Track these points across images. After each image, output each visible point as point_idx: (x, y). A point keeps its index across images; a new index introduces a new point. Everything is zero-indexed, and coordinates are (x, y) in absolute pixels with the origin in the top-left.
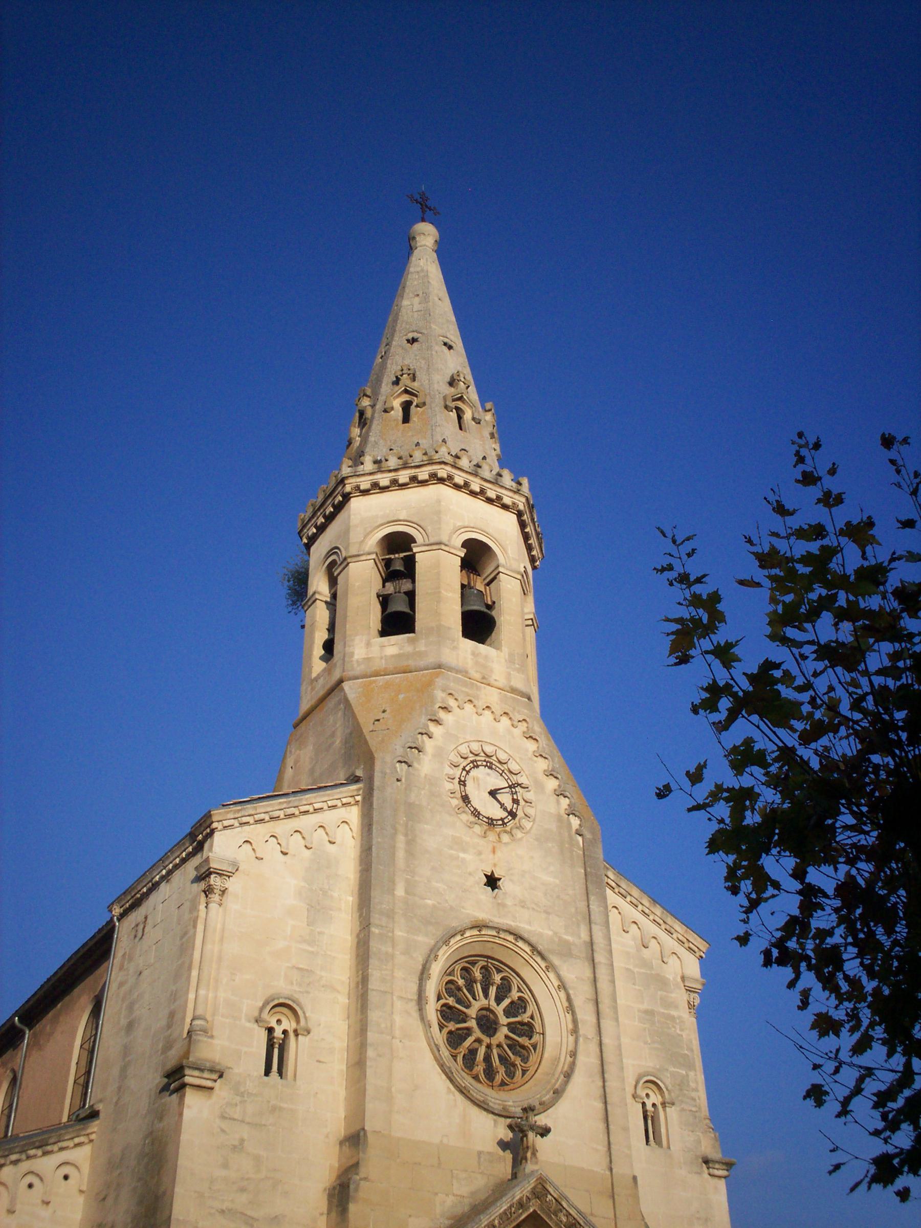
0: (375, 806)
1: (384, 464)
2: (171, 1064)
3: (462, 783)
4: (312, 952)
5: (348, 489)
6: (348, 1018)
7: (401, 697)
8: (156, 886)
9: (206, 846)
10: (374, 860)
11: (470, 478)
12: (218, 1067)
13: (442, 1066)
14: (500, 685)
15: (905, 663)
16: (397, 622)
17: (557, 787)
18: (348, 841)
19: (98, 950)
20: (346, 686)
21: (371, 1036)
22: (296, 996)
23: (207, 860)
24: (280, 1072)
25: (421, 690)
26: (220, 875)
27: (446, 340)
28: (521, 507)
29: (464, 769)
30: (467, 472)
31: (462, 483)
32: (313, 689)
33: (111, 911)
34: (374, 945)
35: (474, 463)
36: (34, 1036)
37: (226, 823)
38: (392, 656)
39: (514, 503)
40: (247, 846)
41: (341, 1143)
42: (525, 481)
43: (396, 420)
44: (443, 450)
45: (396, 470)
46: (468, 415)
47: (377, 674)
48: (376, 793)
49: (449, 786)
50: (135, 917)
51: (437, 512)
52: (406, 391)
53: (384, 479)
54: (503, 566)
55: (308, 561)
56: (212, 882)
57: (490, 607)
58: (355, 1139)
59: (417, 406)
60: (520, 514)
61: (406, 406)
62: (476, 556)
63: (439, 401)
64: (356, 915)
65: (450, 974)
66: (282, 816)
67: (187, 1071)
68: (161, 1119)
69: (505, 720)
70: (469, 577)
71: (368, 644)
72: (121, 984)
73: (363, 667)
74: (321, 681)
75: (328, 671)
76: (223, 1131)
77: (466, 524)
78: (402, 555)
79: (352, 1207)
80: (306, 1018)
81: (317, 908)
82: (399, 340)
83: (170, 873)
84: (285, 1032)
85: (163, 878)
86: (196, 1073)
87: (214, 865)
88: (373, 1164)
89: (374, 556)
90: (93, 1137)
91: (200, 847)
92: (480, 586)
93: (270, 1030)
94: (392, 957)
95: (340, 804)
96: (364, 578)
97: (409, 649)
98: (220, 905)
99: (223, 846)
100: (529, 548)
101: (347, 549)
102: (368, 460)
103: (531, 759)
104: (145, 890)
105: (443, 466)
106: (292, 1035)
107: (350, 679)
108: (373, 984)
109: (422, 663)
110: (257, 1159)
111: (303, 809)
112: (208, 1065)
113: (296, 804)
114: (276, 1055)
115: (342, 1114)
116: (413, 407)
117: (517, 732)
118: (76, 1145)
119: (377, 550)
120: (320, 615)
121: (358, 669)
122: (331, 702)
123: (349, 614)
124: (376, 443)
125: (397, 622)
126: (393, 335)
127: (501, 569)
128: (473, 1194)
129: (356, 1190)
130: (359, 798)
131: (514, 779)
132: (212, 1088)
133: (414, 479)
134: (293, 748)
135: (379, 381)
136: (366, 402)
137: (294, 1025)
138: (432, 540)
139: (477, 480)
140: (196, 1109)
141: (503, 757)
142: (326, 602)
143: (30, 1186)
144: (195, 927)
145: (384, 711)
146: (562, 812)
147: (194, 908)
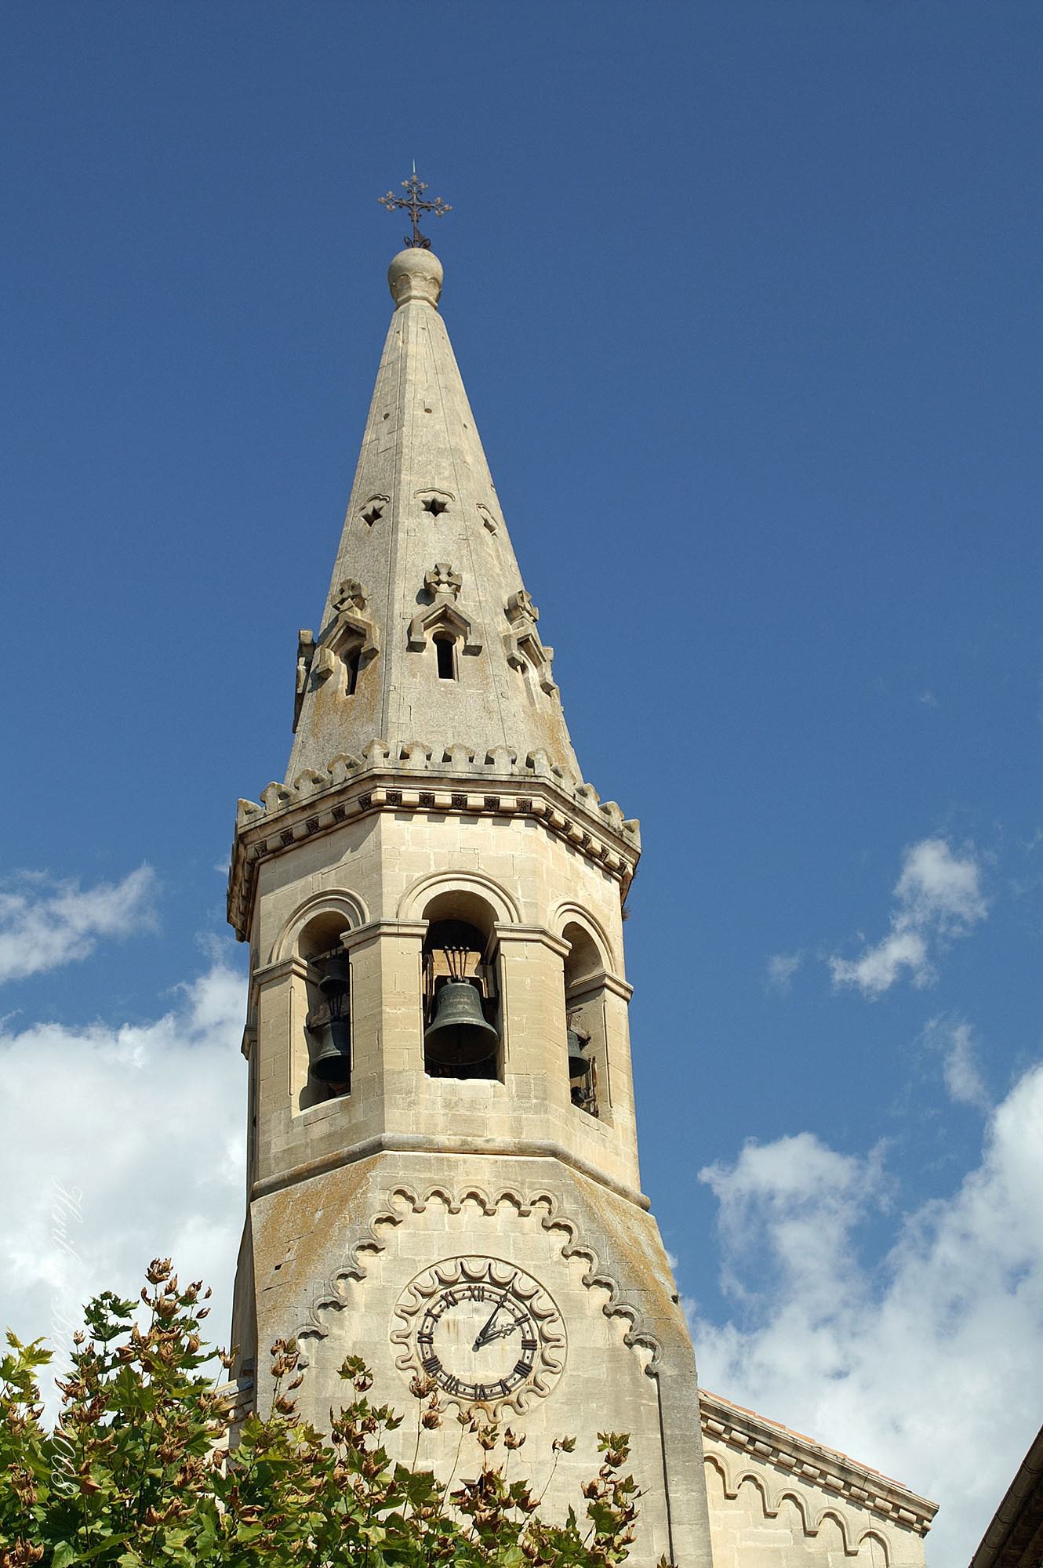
3: (425, 1338)
15: (801, 1208)
77: (433, 870)
82: (355, 520)
97: (342, 1121)
103: (558, 1263)
117: (532, 1222)
146: (620, 1343)
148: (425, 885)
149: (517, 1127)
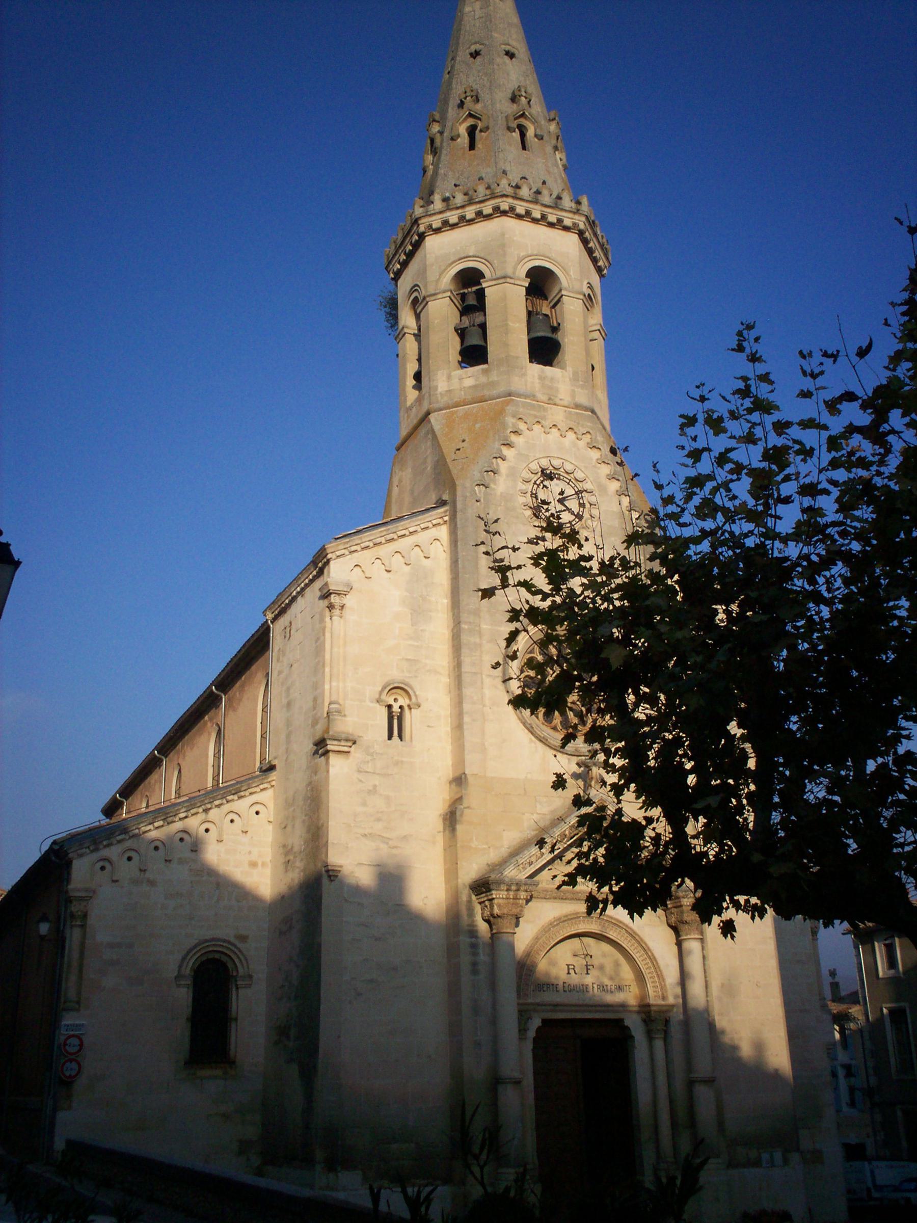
0: (459, 526)
1: (452, 201)
2: (318, 736)
4: (417, 646)
5: (422, 229)
6: (450, 692)
7: (478, 426)
8: (294, 599)
9: (326, 571)
10: (460, 570)
11: (531, 206)
12: (351, 738)
13: (524, 724)
14: (566, 403)
16: (474, 354)
17: (618, 488)
18: (440, 554)
19: (257, 647)
20: (432, 417)
21: (466, 707)
22: (407, 680)
23: (326, 584)
24: (400, 737)
25: (494, 418)
26: (339, 594)
27: (508, 48)
28: (582, 226)
29: (535, 483)
30: (527, 201)
31: (523, 213)
32: (408, 417)
33: (265, 615)
34: (465, 638)
35: (534, 189)
36: (229, 700)
37: (338, 553)
38: (470, 387)
39: (574, 224)
40: (357, 569)
41: (450, 783)
42: (585, 200)
43: (463, 148)
44: (504, 182)
45: (463, 207)
46: (530, 133)
47: (457, 405)
48: (459, 515)
49: (522, 500)
50: (283, 621)
51: (502, 244)
52: (470, 115)
53: (453, 217)
54: (566, 289)
55: (396, 294)
56: (332, 601)
57: (555, 329)
58: (459, 780)
59: (481, 131)
60: (581, 233)
61: (472, 131)
62: (540, 283)
63: (501, 122)
64: (451, 614)
65: (531, 652)
66: (384, 542)
67: (328, 742)
68: (316, 773)
69: (571, 436)
70: (532, 303)
71: (449, 377)
72: (280, 673)
73: (445, 399)
74: (414, 410)
75: (419, 400)
76: (361, 781)
77: (530, 252)
78: (474, 289)
79: (459, 827)
80: (416, 696)
81: (418, 611)
82: (463, 55)
83: (303, 589)
84: (401, 707)
85: (298, 593)
86: (336, 742)
87: (332, 587)
88: (473, 797)
89: (449, 294)
90: (273, 783)
91: (321, 572)
92: (546, 310)
93: (390, 707)
94: (480, 645)
95: (431, 526)
96: (443, 312)
97: (483, 379)
98: (341, 617)
99: (339, 571)
100: (595, 261)
101: (426, 286)
102: (437, 198)
103: (595, 466)
104: (287, 601)
105: (505, 199)
106: (406, 708)
107: (435, 411)
108: (466, 668)
109: (495, 392)
110: (388, 798)
111: (400, 533)
112: (343, 736)
113: (394, 530)
114: (396, 724)
115: (450, 763)
116: (477, 132)
117: (582, 444)
118: (262, 790)
119: (452, 288)
120: (410, 346)
121: (443, 401)
122: (422, 431)
123: (431, 351)
124: (445, 175)
125: (474, 354)
126: (457, 49)
127: (563, 292)
128: (552, 812)
129: (461, 815)
130: (446, 518)
131: (580, 486)
132: (349, 752)
133: (479, 214)
134: (396, 469)
135: (446, 102)
136: (436, 128)
137: (408, 701)
138: (499, 274)
139: (538, 207)
140: (338, 768)
141: (569, 467)
142: (414, 335)
143: (232, 821)
144: (324, 635)
145: (463, 441)
147: (322, 620)
148: (526, 260)
149: (573, 395)
